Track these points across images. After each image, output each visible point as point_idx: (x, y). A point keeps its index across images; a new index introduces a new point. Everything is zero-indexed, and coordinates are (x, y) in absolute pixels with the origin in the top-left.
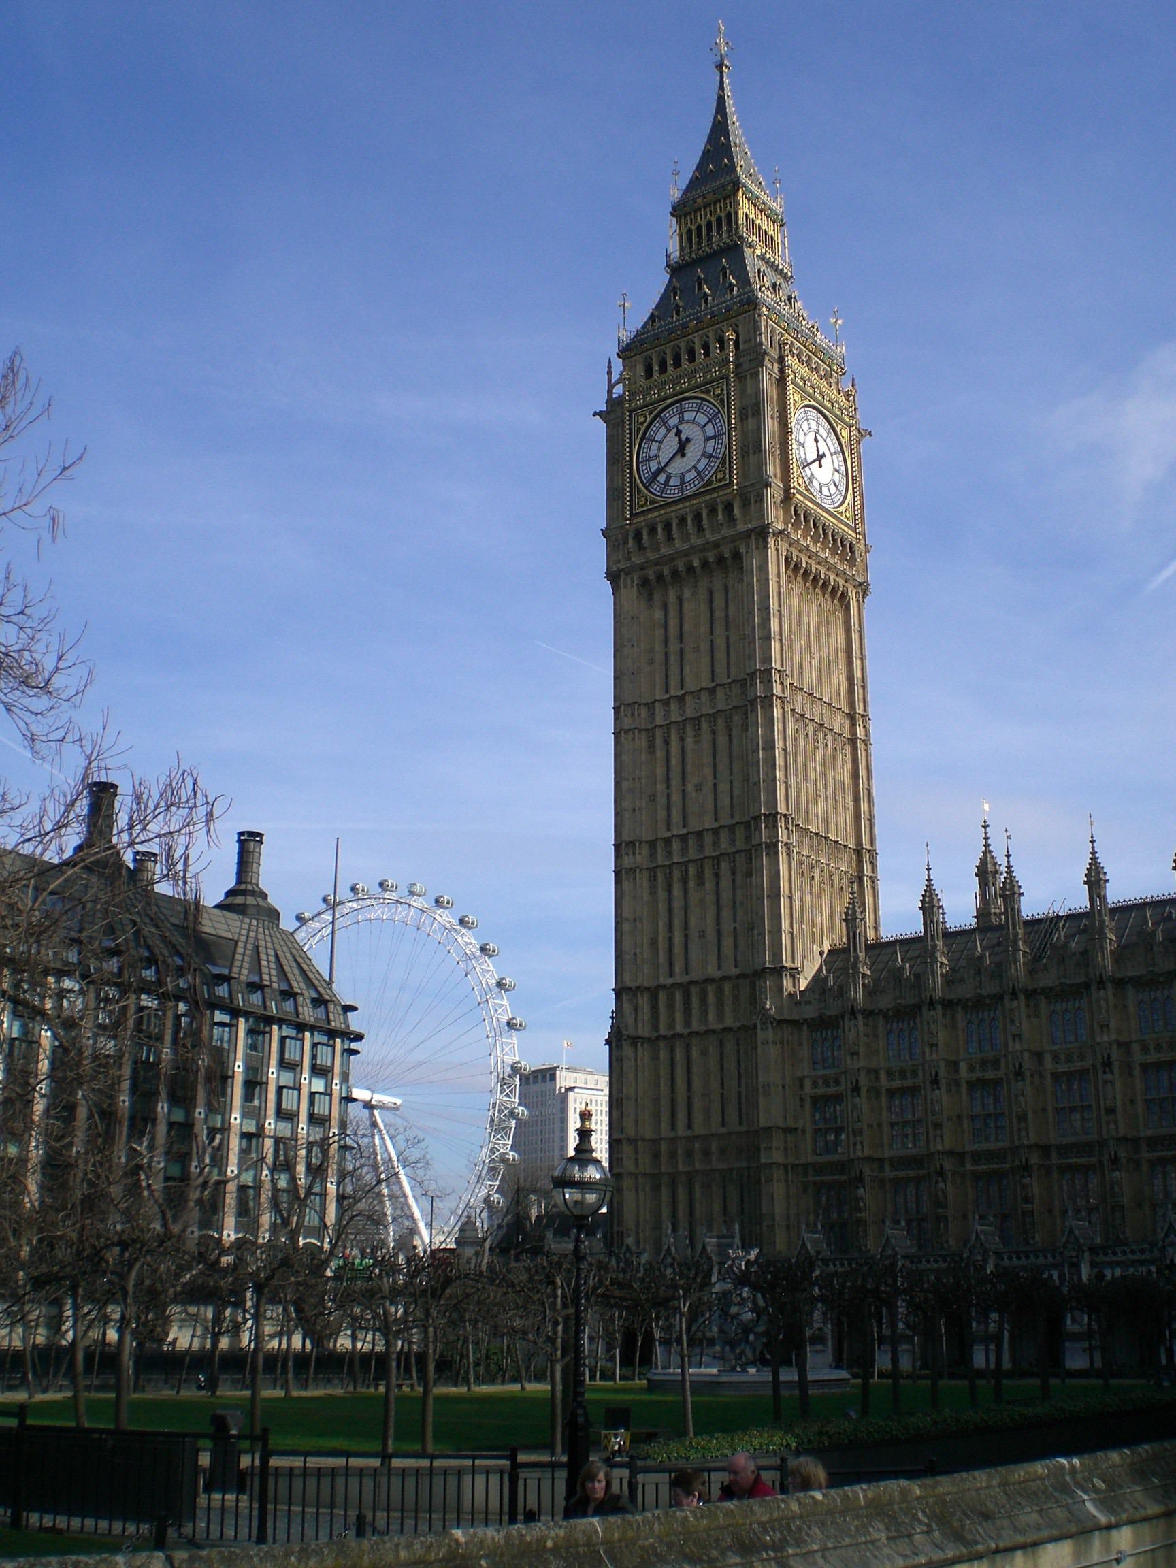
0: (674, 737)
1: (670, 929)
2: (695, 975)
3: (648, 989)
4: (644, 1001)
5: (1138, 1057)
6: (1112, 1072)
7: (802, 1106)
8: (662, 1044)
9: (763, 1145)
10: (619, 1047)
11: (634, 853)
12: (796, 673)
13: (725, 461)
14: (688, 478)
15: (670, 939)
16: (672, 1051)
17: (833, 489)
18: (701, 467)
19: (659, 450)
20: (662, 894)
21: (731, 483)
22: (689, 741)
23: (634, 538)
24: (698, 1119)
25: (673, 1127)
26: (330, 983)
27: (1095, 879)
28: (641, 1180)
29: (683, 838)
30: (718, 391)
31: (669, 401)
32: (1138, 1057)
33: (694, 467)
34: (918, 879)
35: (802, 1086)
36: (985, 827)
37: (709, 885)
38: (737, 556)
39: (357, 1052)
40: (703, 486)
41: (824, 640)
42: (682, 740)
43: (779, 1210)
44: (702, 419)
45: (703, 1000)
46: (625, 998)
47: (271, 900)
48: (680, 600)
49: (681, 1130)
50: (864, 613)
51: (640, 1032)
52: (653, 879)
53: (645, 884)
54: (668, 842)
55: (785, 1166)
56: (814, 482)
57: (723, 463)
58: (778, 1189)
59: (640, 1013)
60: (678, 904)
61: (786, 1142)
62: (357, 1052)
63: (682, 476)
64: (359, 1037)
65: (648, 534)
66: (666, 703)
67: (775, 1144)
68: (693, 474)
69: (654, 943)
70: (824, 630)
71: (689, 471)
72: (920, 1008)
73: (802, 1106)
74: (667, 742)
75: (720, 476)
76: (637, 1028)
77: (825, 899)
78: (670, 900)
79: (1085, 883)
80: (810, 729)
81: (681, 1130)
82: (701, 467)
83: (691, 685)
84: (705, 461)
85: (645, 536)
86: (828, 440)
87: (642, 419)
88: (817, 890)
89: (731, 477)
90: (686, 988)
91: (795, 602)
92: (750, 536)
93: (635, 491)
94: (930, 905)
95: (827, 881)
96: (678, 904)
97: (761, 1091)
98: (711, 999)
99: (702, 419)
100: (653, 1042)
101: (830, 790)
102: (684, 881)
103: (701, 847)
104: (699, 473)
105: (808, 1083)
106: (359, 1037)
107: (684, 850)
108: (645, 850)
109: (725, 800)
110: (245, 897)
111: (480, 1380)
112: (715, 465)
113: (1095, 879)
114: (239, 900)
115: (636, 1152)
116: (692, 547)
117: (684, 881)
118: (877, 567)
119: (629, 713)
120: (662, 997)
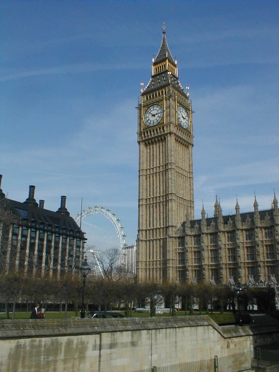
0: (151, 177)
1: (150, 217)
2: (155, 227)
3: (145, 230)
4: (144, 232)
5: (265, 243)
6: (239, 248)
7: (176, 255)
8: (158, 240)
9: (168, 262)
10: (139, 242)
11: (142, 201)
12: (177, 164)
13: (163, 118)
14: (155, 122)
15: (150, 220)
16: (153, 242)
17: (186, 124)
18: (157, 119)
19: (149, 115)
20: (148, 210)
21: (164, 123)
22: (154, 178)
23: (143, 134)
24: (155, 257)
25: (150, 259)
26: (80, 228)
27: (256, 205)
28: (143, 270)
29: (153, 198)
30: (161, 103)
31: (151, 105)
32: (265, 243)
33: (156, 119)
34: (203, 207)
35: (176, 251)
36: (216, 196)
37: (158, 208)
38: (165, 138)
39: (86, 242)
40: (158, 123)
41: (184, 156)
42: (153, 177)
43: (171, 276)
44: (158, 109)
45: (153, 233)
46: (140, 232)
47: (68, 210)
48: (153, 147)
49: (151, 260)
50: (192, 150)
51: (143, 239)
52: (146, 207)
53: (145, 208)
54: (149, 199)
55: (172, 267)
56: (182, 123)
57: (162, 118)
58: (171, 272)
59: (143, 235)
60: (151, 212)
61: (172, 262)
62: (86, 242)
63: (154, 121)
64: (86, 239)
65: (159, 129)
66: (150, 169)
67: (170, 263)
68: (156, 121)
69: (146, 220)
70: (184, 154)
71: (155, 120)
72: (185, 236)
73: (176, 255)
74: (150, 178)
75: (162, 121)
76: (142, 238)
77: (183, 211)
78: (160, 209)
79: (254, 206)
80: (180, 175)
81: (151, 260)
82: (157, 119)
83: (155, 166)
84: (158, 118)
85: (158, 129)
86: (185, 114)
87: (145, 109)
88: (181, 209)
89: (164, 121)
90: (153, 230)
91: (177, 148)
92: (167, 134)
93: (144, 124)
94: (203, 213)
95: (183, 208)
96: (151, 212)
97: (167, 252)
98: (158, 232)
99: (158, 109)
100: (146, 241)
101: (184, 188)
102: (153, 207)
103: (156, 200)
104: (157, 121)
105: (177, 250)
106: (86, 239)
107: (153, 201)
108: (145, 201)
109: (162, 190)
110: (63, 209)
111: (112, 310)
112: (160, 119)
113: (256, 205)
114: (61, 210)
115: (142, 264)
116: (159, 135)
117: (153, 207)
118: (195, 141)
119: (142, 171)
120: (148, 231)
